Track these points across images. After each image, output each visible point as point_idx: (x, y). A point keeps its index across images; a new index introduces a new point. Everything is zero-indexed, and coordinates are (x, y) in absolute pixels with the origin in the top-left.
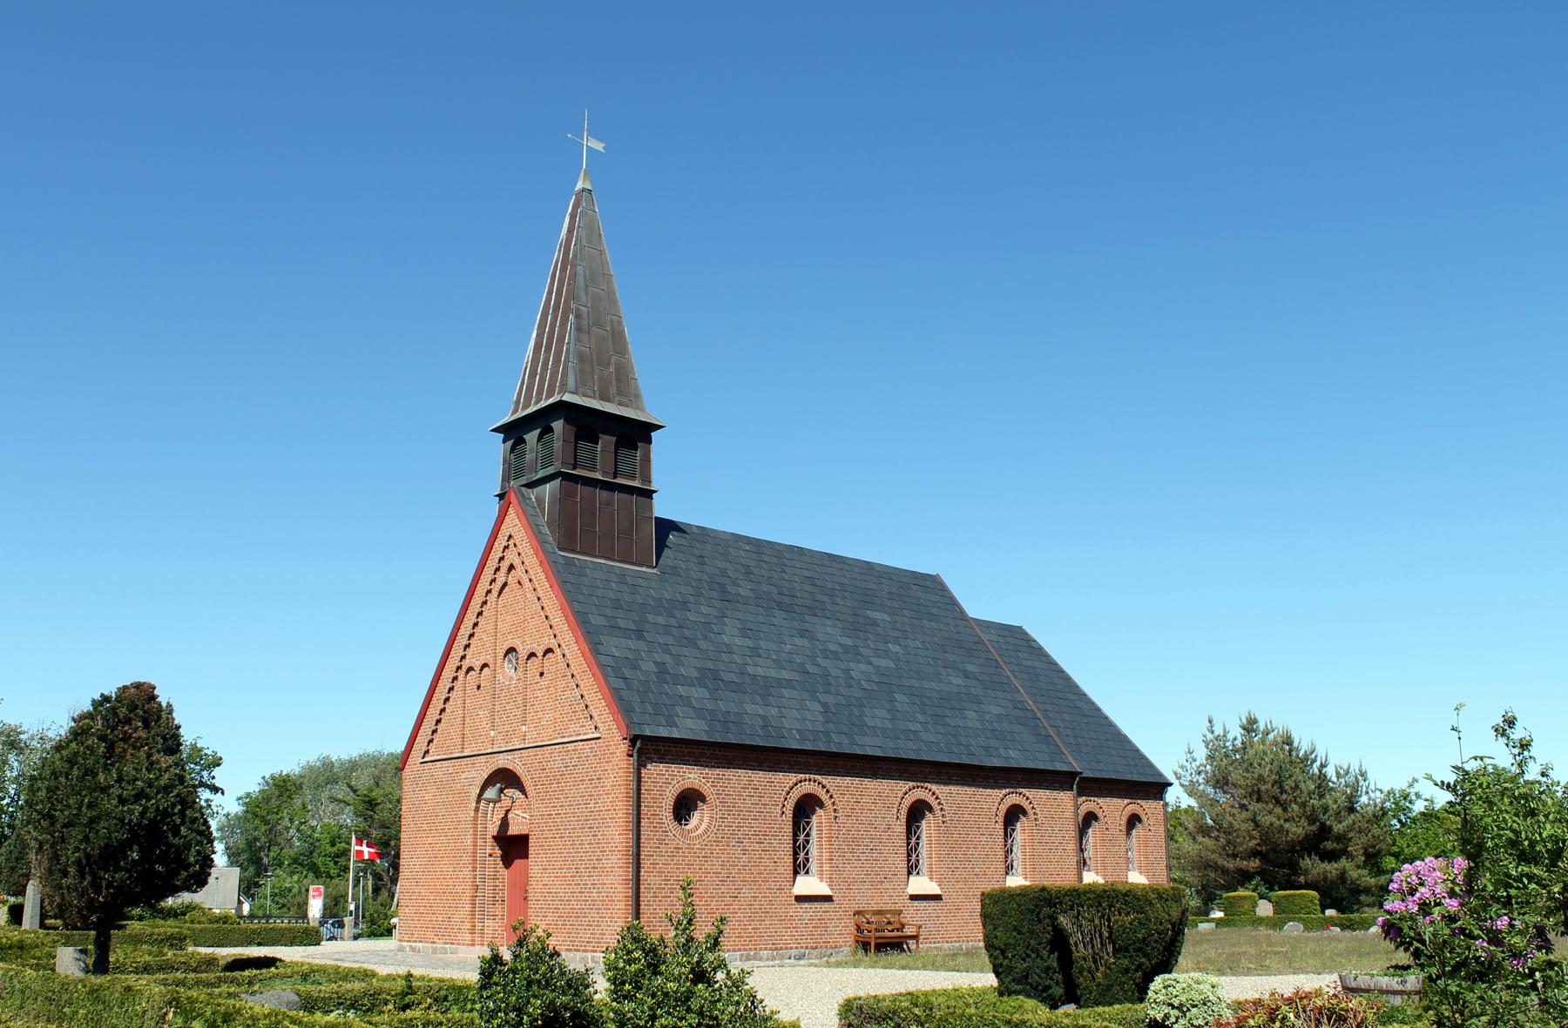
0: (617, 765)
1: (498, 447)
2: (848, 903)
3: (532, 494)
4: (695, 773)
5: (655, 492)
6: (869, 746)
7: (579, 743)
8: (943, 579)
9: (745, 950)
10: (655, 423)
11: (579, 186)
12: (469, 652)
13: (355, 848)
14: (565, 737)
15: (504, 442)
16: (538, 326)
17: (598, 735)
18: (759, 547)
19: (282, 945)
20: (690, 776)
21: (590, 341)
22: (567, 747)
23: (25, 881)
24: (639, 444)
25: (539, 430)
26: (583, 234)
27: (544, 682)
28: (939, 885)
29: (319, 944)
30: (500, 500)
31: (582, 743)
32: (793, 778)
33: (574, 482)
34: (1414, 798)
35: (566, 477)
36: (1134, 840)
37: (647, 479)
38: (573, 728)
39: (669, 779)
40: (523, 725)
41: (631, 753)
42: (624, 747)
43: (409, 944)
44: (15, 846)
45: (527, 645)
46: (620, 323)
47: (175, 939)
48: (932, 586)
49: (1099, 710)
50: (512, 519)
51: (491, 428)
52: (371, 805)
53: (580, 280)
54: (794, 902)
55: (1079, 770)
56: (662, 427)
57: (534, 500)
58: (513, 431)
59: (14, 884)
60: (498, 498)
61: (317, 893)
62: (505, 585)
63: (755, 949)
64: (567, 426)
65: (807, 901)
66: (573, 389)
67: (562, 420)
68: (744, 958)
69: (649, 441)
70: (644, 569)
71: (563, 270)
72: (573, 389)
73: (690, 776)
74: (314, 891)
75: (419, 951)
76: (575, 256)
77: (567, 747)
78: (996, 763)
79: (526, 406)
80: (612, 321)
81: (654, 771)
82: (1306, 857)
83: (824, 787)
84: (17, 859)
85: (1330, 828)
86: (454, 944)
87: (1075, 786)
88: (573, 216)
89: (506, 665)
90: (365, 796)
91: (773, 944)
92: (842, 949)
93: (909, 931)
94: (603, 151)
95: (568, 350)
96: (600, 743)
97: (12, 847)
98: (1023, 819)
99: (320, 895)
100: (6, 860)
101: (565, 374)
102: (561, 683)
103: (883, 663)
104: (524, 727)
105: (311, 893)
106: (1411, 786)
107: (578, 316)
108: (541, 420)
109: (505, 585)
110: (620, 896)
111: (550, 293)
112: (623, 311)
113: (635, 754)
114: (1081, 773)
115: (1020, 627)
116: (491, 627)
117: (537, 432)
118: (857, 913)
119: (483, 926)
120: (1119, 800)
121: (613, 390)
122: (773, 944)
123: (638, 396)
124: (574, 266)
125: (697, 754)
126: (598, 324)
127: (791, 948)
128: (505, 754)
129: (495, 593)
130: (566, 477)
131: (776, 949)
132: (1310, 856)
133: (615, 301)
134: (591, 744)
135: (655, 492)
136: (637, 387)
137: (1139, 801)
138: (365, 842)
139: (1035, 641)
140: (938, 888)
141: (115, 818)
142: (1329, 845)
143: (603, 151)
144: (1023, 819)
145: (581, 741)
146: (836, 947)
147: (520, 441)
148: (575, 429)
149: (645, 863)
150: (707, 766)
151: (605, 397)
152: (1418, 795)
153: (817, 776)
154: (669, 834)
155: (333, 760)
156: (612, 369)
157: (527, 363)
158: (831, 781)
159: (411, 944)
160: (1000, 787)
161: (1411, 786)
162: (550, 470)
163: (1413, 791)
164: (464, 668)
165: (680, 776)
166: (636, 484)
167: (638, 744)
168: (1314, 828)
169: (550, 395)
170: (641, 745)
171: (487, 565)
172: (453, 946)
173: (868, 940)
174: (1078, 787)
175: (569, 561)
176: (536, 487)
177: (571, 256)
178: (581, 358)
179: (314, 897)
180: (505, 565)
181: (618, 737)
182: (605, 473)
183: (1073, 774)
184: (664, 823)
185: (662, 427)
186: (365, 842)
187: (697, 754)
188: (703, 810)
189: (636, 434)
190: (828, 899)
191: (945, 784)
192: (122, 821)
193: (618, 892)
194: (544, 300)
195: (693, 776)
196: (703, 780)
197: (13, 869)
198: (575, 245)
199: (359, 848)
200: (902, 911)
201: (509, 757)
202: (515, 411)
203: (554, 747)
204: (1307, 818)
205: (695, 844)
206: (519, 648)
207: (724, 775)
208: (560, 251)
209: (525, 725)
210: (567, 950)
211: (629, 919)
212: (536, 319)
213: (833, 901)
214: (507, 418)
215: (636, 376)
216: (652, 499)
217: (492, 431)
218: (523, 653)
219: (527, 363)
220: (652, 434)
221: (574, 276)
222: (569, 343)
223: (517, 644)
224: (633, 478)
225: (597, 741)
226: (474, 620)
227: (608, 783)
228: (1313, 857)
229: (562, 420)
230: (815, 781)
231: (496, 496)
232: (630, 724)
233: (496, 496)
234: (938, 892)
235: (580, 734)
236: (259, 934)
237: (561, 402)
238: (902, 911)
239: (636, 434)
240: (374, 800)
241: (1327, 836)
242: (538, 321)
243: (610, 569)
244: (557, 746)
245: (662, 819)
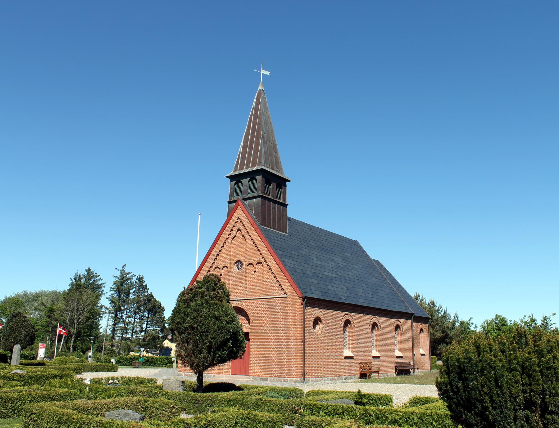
0: (296, 307)
1: (228, 184)
2: (358, 360)
3: (247, 203)
4: (319, 311)
5: (288, 205)
6: (361, 302)
7: (276, 298)
8: (359, 243)
9: (331, 376)
10: (288, 179)
11: (260, 88)
12: (216, 261)
13: (59, 329)
14: (268, 296)
15: (231, 181)
16: (244, 139)
17: (286, 296)
18: (311, 227)
19: (104, 372)
20: (317, 312)
21: (267, 147)
22: (271, 300)
23: (12, 345)
24: (283, 187)
25: (249, 179)
26: (263, 106)
27: (255, 274)
28: (379, 353)
29: (116, 371)
30: (229, 204)
31: (278, 299)
32: (344, 313)
33: (265, 199)
34: (471, 324)
35: (263, 198)
36: (347, 333)
37: (285, 200)
38: (272, 292)
39: (315, 312)
40: (245, 290)
41: (302, 303)
42: (300, 301)
43: (184, 373)
44: (7, 330)
45: (248, 260)
46: (275, 141)
47: (77, 370)
48: (354, 245)
49: (406, 291)
50: (239, 213)
51: (225, 176)
52: (52, 311)
53: (263, 123)
54: (344, 359)
55: (413, 313)
56: (290, 181)
57: (247, 205)
58: (236, 179)
59: (7, 346)
60: (228, 203)
61: (43, 347)
62: (235, 236)
63: (334, 376)
64: (263, 178)
65: (347, 359)
66: (263, 164)
67: (261, 176)
68: (331, 380)
69: (285, 186)
70: (285, 234)
71: (255, 118)
72: (263, 164)
73: (317, 312)
74: (41, 346)
75: (190, 376)
76: (260, 114)
77: (271, 300)
78: (393, 309)
79: (241, 168)
80: (273, 140)
81: (309, 309)
82: (441, 344)
83: (351, 317)
84: (9, 336)
85: (449, 334)
86: (209, 373)
87: (412, 318)
88: (258, 99)
89: (235, 267)
90: (50, 308)
91: (339, 374)
92: (356, 376)
93: (374, 369)
94: (269, 75)
95: (261, 149)
96: (287, 299)
97: (5, 331)
98: (349, 326)
99: (44, 347)
100: (3, 336)
101: (260, 159)
102: (266, 276)
103: (355, 272)
104: (246, 291)
105: (40, 346)
106: (470, 320)
107: (263, 137)
108: (251, 175)
109: (235, 236)
110: (298, 357)
111: (249, 127)
112: (276, 137)
113: (304, 304)
114: (414, 314)
115: (378, 261)
116: (228, 252)
117: (248, 179)
118: (361, 363)
119: (223, 367)
120: (418, 324)
121: (275, 166)
122: (339, 374)
123: (282, 169)
124: (260, 118)
125: (320, 304)
126: (269, 141)
127: (343, 376)
128: (237, 301)
129: (230, 239)
130: (263, 198)
131: (339, 376)
132: (443, 344)
133: (273, 133)
134: (283, 299)
135: (288, 205)
136: (281, 166)
137: (423, 324)
138: (62, 327)
139: (383, 266)
140: (379, 354)
141: (226, 329)
142: (448, 340)
143: (269, 75)
144: (349, 326)
145: (271, 298)
146: (354, 375)
147: (239, 182)
148: (265, 179)
149: (306, 344)
150: (322, 309)
151: (273, 169)
152: (472, 324)
153: (348, 313)
154: (312, 333)
155: (28, 292)
156: (274, 158)
157: (240, 150)
158: (380, 319)
159: (185, 373)
160: (394, 318)
161: (470, 320)
162: (255, 194)
163: (471, 322)
164: (214, 267)
165: (315, 312)
166: (281, 201)
167: (306, 300)
168: (443, 335)
169: (254, 165)
170: (307, 300)
171: (226, 228)
172: (209, 374)
173: (366, 373)
174: (413, 319)
175: (265, 229)
176: (248, 200)
177: (258, 114)
178: (265, 153)
179: (41, 348)
180: (235, 229)
181: (296, 297)
182: (273, 197)
183: (412, 314)
184: (311, 330)
185: (290, 181)
186: (62, 327)
187: (320, 304)
188: (320, 325)
189: (282, 183)
190: (352, 358)
191: (381, 317)
192: (228, 331)
193: (297, 355)
194: (246, 129)
195: (318, 312)
196: (321, 314)
197: (6, 340)
198: (260, 110)
199: (60, 329)
200: (372, 362)
201: (239, 303)
202: (235, 170)
203: (263, 299)
204: (441, 331)
205: (319, 337)
206: (243, 261)
207: (326, 312)
208: (252, 111)
209: (247, 290)
210: (270, 377)
211: (302, 365)
212: (243, 136)
213: (353, 358)
214: (231, 173)
215: (281, 162)
216: (287, 207)
217: (225, 177)
218: (245, 264)
219: (240, 150)
220: (286, 183)
221: (260, 122)
222: (261, 147)
223: (252, 261)
224: (280, 199)
225: (286, 298)
226: (219, 249)
227: (292, 315)
228: (444, 344)
229: (261, 176)
230: (349, 315)
231: (227, 202)
232: (302, 293)
233: (227, 202)
234: (379, 355)
235: (276, 295)
236: (96, 367)
237: (262, 169)
238: (372, 362)
239: (282, 183)
240: (53, 309)
241: (447, 337)
242: (244, 137)
243: (276, 234)
244: (265, 299)
245: (310, 328)
